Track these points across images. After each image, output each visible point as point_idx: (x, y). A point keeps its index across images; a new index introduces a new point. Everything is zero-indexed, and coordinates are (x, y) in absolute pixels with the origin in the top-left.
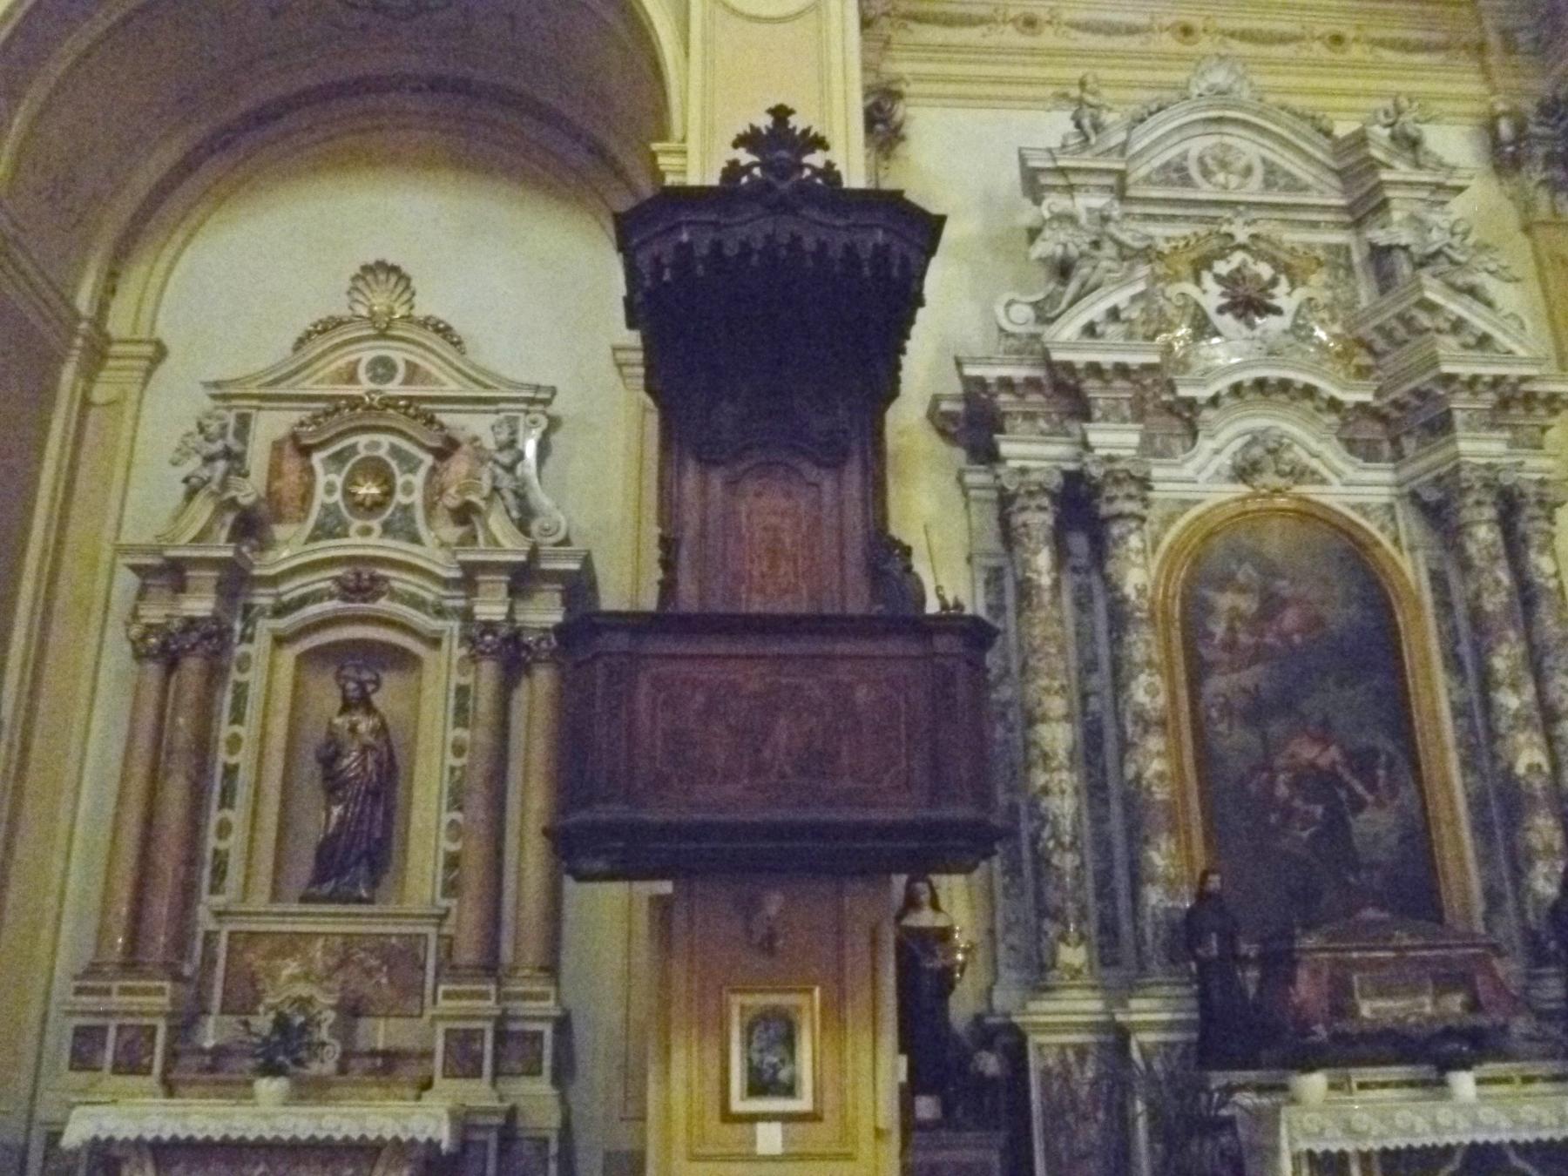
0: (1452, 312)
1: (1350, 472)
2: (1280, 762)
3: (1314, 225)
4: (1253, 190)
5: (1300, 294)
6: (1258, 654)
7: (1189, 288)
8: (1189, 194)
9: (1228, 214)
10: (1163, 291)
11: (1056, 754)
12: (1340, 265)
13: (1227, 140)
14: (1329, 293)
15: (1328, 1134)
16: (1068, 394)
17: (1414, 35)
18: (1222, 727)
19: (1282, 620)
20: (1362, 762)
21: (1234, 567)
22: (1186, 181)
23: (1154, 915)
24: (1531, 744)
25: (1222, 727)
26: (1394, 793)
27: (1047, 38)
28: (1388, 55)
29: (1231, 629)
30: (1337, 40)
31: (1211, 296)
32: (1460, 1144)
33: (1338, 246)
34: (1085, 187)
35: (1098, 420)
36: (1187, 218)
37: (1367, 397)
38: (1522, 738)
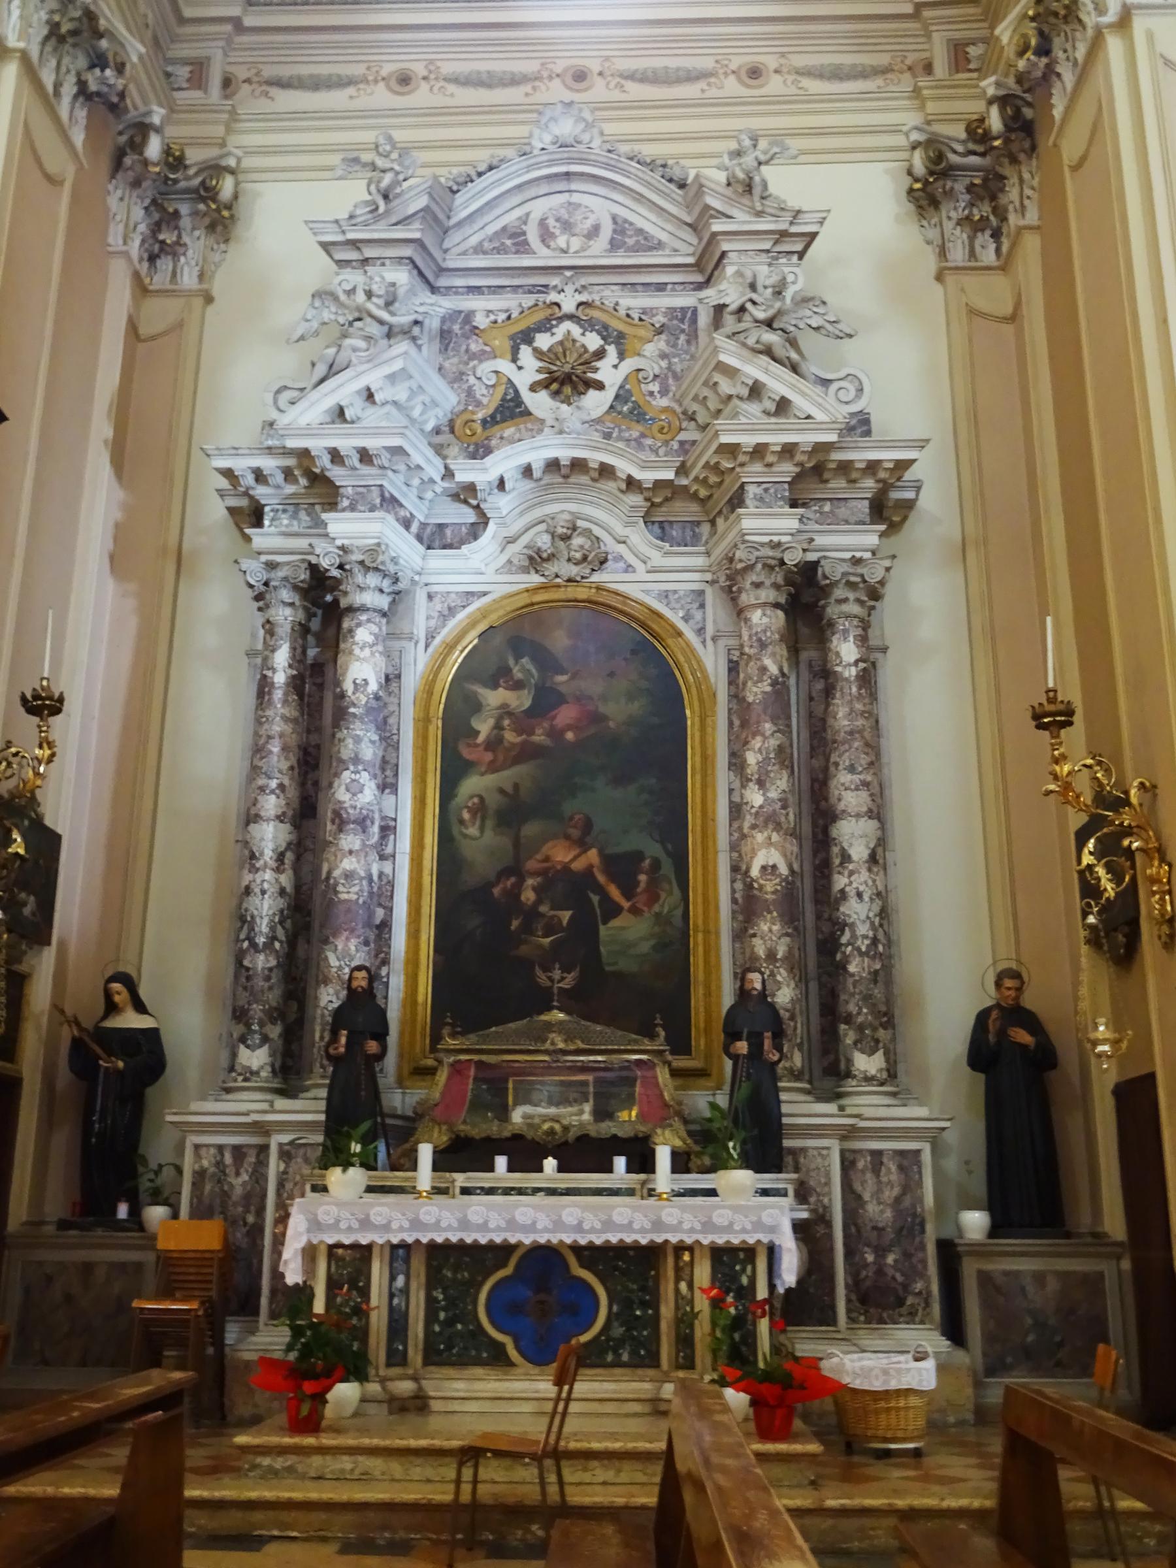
0: (748, 376)
1: (657, 559)
2: (531, 865)
3: (661, 287)
4: (598, 252)
5: (629, 365)
6: (526, 753)
7: (505, 366)
8: (527, 261)
9: (555, 281)
10: (474, 368)
11: (262, 854)
12: (683, 331)
13: (576, 198)
14: (664, 364)
15: (343, 1225)
16: (317, 486)
17: (848, 60)
18: (473, 831)
19: (554, 718)
20: (623, 867)
21: (511, 662)
22: (522, 246)
23: (323, 1016)
24: (769, 843)
25: (473, 831)
26: (653, 898)
27: (422, 96)
28: (815, 86)
29: (498, 727)
30: (755, 73)
31: (526, 371)
32: (519, 1245)
33: (683, 310)
34: (382, 261)
35: (343, 510)
36: (515, 288)
37: (669, 475)
38: (760, 837)
